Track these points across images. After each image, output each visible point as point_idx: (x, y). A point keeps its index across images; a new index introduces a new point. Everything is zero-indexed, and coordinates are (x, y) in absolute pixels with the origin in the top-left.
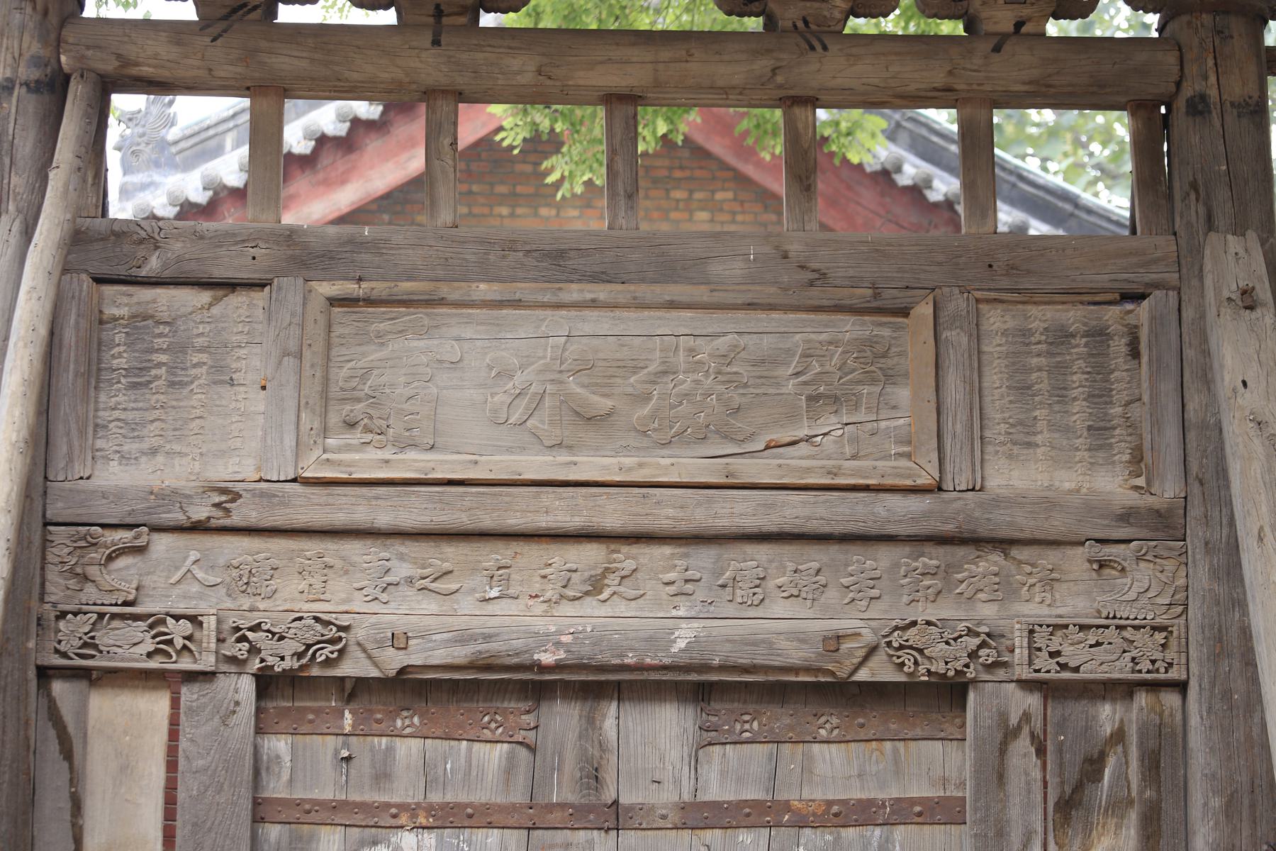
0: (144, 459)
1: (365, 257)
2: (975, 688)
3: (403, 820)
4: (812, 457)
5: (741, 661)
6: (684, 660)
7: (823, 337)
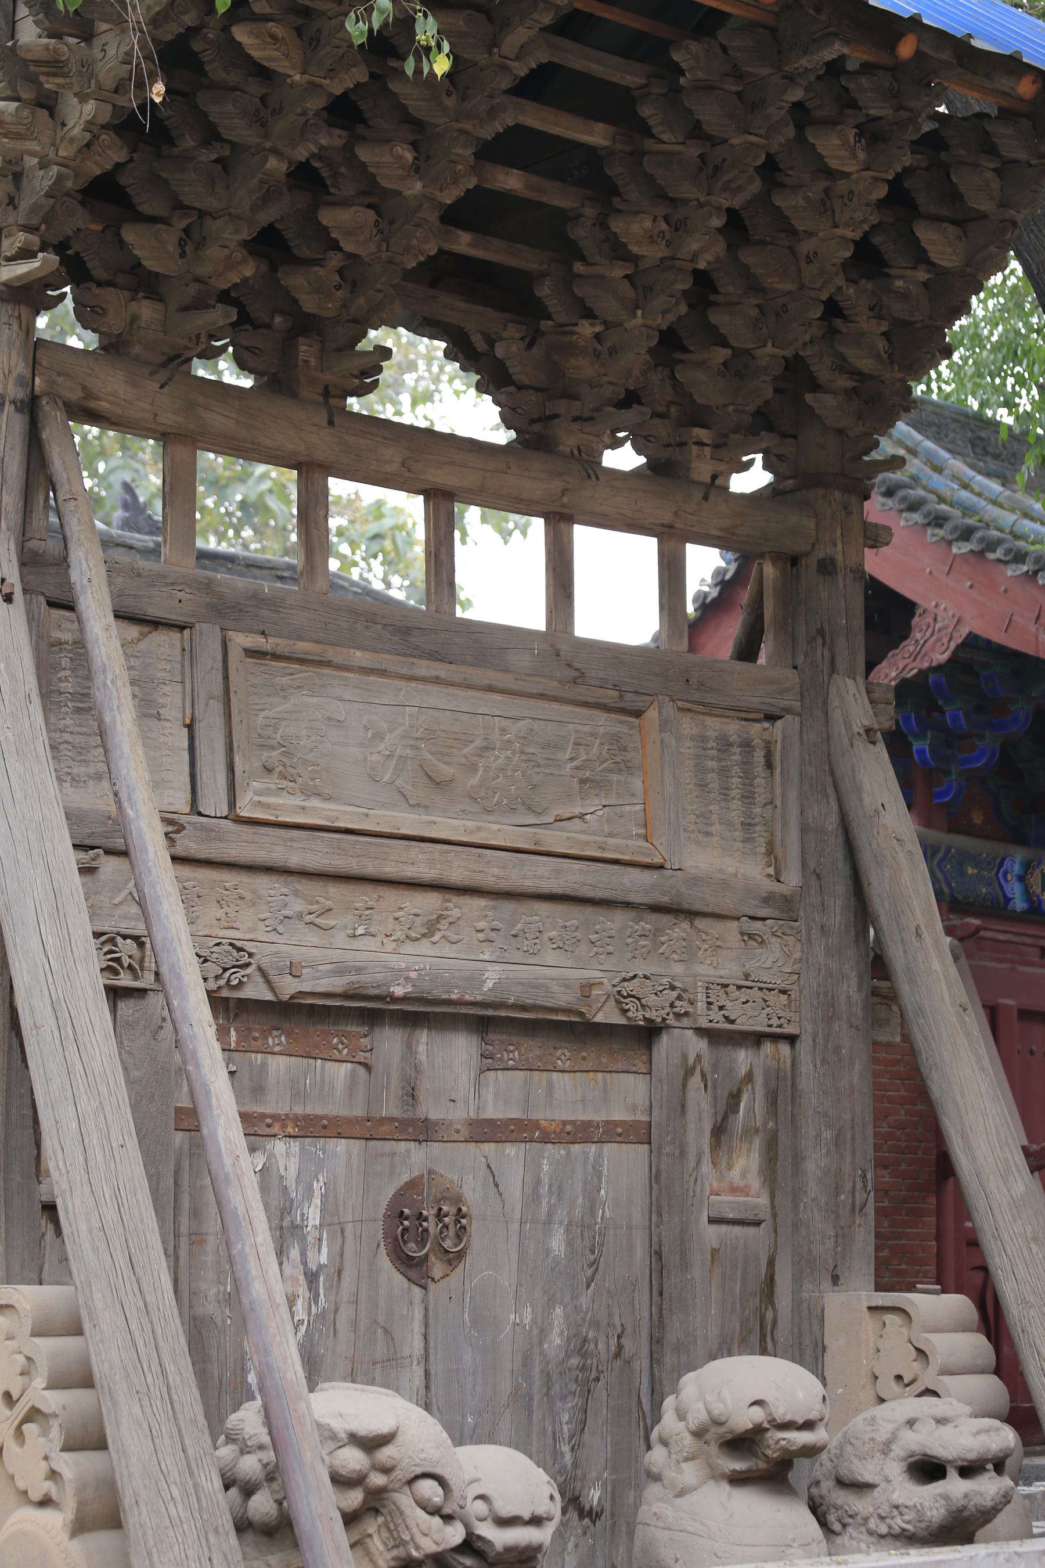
0: (91, 783)
1: (265, 613)
2: (668, 1033)
3: (276, 1129)
4: (583, 832)
5: (528, 1001)
6: (489, 999)
7: (587, 729)
